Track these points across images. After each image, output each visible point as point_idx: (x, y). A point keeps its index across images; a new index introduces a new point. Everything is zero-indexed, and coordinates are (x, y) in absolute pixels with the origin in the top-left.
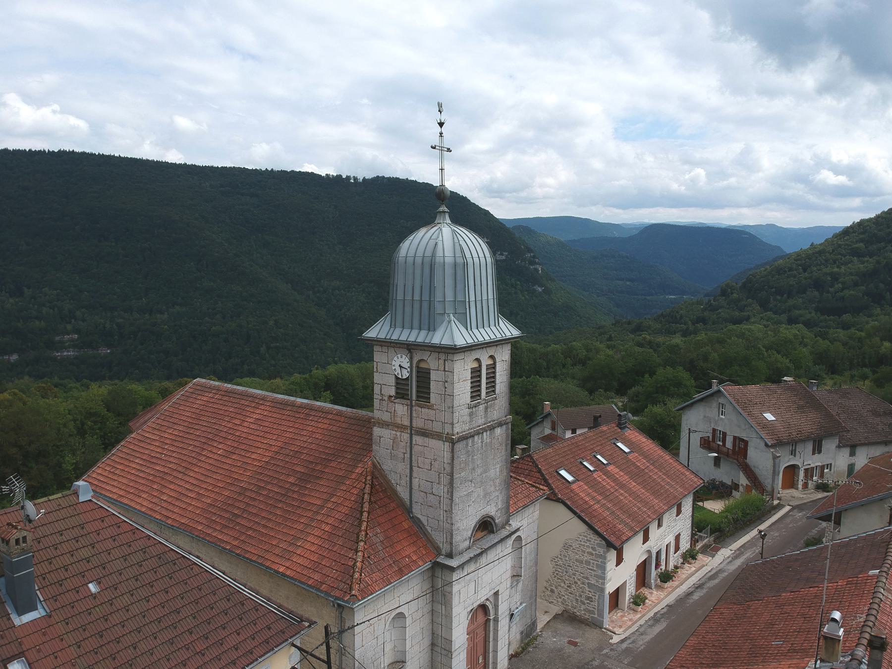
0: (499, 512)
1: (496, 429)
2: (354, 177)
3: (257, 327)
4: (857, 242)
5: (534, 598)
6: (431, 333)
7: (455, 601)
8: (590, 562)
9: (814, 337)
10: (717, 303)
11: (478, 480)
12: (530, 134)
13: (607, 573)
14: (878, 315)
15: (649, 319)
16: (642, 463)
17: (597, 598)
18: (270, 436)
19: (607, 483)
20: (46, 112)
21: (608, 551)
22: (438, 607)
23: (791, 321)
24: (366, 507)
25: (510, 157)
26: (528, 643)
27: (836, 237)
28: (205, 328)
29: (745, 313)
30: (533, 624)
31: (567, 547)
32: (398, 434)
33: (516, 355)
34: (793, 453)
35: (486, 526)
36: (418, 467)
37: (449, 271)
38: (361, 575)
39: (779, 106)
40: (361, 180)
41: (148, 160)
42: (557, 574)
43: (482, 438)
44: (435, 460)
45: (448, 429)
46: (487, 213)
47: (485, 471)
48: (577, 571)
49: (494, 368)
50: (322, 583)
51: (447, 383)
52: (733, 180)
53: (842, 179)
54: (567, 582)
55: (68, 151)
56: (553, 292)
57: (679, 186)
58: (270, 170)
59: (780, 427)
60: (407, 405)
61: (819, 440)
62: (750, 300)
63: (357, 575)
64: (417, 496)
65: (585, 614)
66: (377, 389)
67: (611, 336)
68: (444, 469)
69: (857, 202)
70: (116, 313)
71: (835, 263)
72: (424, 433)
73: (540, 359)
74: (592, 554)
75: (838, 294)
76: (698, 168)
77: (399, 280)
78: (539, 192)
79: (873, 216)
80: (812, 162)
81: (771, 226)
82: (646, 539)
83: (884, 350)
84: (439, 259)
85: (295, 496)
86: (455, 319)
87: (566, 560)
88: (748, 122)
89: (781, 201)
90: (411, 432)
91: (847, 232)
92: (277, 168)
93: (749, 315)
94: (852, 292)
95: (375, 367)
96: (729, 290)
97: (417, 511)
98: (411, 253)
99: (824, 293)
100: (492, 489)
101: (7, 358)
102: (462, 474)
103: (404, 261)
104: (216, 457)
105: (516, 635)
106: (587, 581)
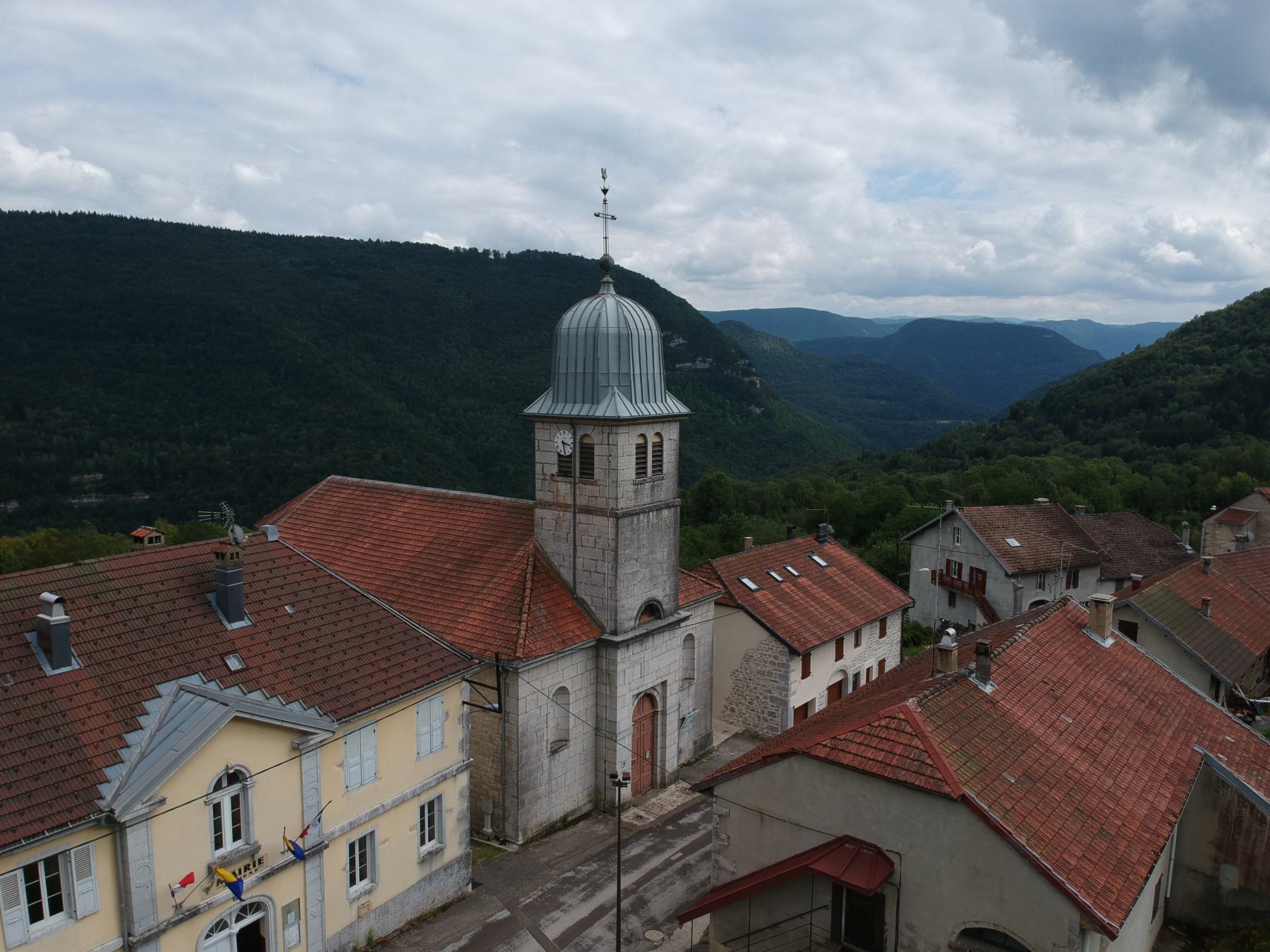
0: (667, 598)
1: (663, 511)
2: (494, 251)
3: (358, 463)
4: (1200, 344)
5: (709, 707)
6: (595, 406)
7: (620, 681)
8: (772, 673)
9: (1131, 472)
10: (1004, 429)
11: (644, 560)
12: (746, 191)
13: (792, 684)
14: (1228, 444)
15: (910, 452)
16: (841, 578)
17: (780, 713)
18: (422, 528)
19: (799, 596)
20: (50, 157)
21: (791, 659)
22: (603, 689)
23: (1106, 453)
24: (529, 584)
25: (717, 223)
26: (703, 754)
27: (1171, 337)
28: (284, 464)
29: (1043, 443)
30: (708, 738)
31: (747, 658)
32: (561, 513)
33: (719, 495)
34: (1041, 586)
35: (651, 609)
36: (582, 546)
37: (613, 343)
38: (525, 642)
39: (1099, 152)
40: (505, 256)
41: (201, 227)
42: (738, 690)
43: (648, 517)
44: (599, 537)
45: (612, 504)
46: (683, 303)
47: (652, 552)
48: (759, 685)
49: (661, 446)
50: (486, 651)
51: (611, 456)
52: (1032, 258)
53: (1187, 256)
54: (748, 698)
55: (87, 213)
56: (777, 415)
57: (957, 265)
58: (375, 241)
59: (1025, 555)
60: (570, 483)
61: (1074, 572)
62: (1051, 425)
63: (521, 641)
64: (581, 576)
65: (767, 732)
66: (538, 468)
67: (855, 474)
68: (609, 545)
69: (1207, 288)
70: (157, 443)
71: (1169, 373)
72: (588, 511)
73: (751, 499)
74: (775, 664)
75: (1172, 416)
76: (984, 239)
77: (562, 352)
78: (759, 273)
79: (1223, 307)
80: (1146, 232)
81: (1086, 323)
82: (839, 655)
83: (1222, 488)
84: (602, 330)
85: (453, 580)
86: (620, 393)
87: (747, 673)
88: (1057, 174)
89: (1099, 286)
90: (574, 510)
91: (1186, 330)
92: (385, 238)
93: (1048, 446)
94: (1192, 414)
95: (537, 444)
96: (1022, 411)
97: (581, 592)
98: (574, 325)
99: (1154, 415)
100: (660, 572)
101: (3, 506)
102: (627, 551)
103: (566, 333)
104: (362, 551)
105: (688, 742)
106: (769, 695)
